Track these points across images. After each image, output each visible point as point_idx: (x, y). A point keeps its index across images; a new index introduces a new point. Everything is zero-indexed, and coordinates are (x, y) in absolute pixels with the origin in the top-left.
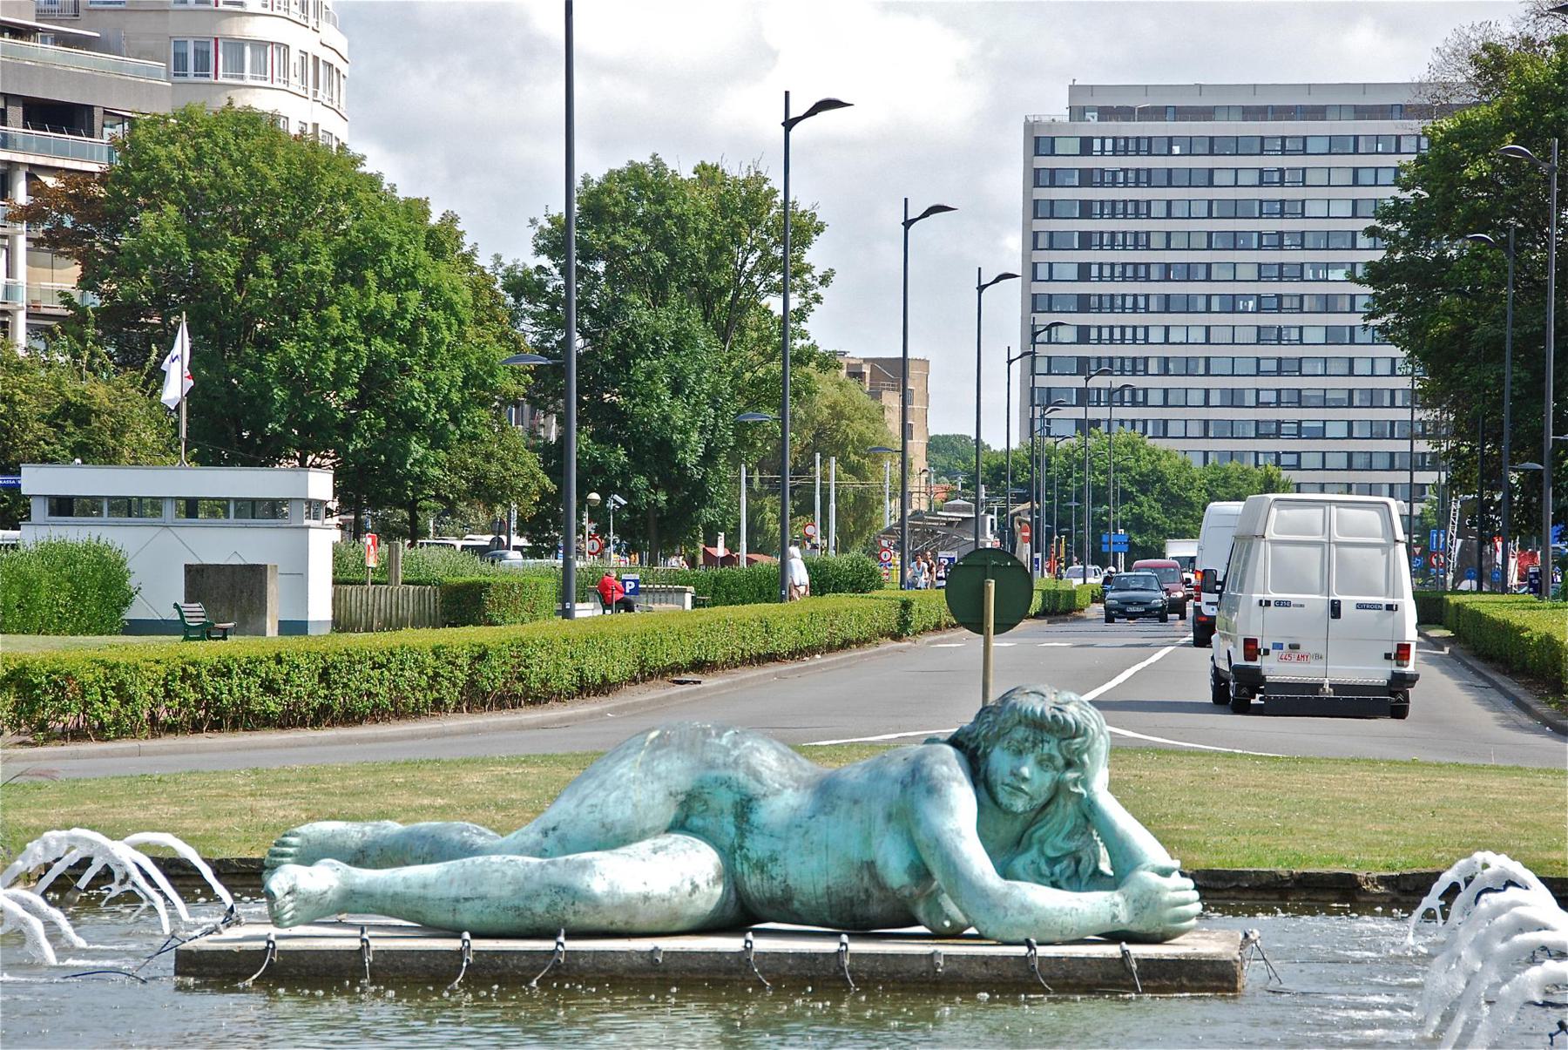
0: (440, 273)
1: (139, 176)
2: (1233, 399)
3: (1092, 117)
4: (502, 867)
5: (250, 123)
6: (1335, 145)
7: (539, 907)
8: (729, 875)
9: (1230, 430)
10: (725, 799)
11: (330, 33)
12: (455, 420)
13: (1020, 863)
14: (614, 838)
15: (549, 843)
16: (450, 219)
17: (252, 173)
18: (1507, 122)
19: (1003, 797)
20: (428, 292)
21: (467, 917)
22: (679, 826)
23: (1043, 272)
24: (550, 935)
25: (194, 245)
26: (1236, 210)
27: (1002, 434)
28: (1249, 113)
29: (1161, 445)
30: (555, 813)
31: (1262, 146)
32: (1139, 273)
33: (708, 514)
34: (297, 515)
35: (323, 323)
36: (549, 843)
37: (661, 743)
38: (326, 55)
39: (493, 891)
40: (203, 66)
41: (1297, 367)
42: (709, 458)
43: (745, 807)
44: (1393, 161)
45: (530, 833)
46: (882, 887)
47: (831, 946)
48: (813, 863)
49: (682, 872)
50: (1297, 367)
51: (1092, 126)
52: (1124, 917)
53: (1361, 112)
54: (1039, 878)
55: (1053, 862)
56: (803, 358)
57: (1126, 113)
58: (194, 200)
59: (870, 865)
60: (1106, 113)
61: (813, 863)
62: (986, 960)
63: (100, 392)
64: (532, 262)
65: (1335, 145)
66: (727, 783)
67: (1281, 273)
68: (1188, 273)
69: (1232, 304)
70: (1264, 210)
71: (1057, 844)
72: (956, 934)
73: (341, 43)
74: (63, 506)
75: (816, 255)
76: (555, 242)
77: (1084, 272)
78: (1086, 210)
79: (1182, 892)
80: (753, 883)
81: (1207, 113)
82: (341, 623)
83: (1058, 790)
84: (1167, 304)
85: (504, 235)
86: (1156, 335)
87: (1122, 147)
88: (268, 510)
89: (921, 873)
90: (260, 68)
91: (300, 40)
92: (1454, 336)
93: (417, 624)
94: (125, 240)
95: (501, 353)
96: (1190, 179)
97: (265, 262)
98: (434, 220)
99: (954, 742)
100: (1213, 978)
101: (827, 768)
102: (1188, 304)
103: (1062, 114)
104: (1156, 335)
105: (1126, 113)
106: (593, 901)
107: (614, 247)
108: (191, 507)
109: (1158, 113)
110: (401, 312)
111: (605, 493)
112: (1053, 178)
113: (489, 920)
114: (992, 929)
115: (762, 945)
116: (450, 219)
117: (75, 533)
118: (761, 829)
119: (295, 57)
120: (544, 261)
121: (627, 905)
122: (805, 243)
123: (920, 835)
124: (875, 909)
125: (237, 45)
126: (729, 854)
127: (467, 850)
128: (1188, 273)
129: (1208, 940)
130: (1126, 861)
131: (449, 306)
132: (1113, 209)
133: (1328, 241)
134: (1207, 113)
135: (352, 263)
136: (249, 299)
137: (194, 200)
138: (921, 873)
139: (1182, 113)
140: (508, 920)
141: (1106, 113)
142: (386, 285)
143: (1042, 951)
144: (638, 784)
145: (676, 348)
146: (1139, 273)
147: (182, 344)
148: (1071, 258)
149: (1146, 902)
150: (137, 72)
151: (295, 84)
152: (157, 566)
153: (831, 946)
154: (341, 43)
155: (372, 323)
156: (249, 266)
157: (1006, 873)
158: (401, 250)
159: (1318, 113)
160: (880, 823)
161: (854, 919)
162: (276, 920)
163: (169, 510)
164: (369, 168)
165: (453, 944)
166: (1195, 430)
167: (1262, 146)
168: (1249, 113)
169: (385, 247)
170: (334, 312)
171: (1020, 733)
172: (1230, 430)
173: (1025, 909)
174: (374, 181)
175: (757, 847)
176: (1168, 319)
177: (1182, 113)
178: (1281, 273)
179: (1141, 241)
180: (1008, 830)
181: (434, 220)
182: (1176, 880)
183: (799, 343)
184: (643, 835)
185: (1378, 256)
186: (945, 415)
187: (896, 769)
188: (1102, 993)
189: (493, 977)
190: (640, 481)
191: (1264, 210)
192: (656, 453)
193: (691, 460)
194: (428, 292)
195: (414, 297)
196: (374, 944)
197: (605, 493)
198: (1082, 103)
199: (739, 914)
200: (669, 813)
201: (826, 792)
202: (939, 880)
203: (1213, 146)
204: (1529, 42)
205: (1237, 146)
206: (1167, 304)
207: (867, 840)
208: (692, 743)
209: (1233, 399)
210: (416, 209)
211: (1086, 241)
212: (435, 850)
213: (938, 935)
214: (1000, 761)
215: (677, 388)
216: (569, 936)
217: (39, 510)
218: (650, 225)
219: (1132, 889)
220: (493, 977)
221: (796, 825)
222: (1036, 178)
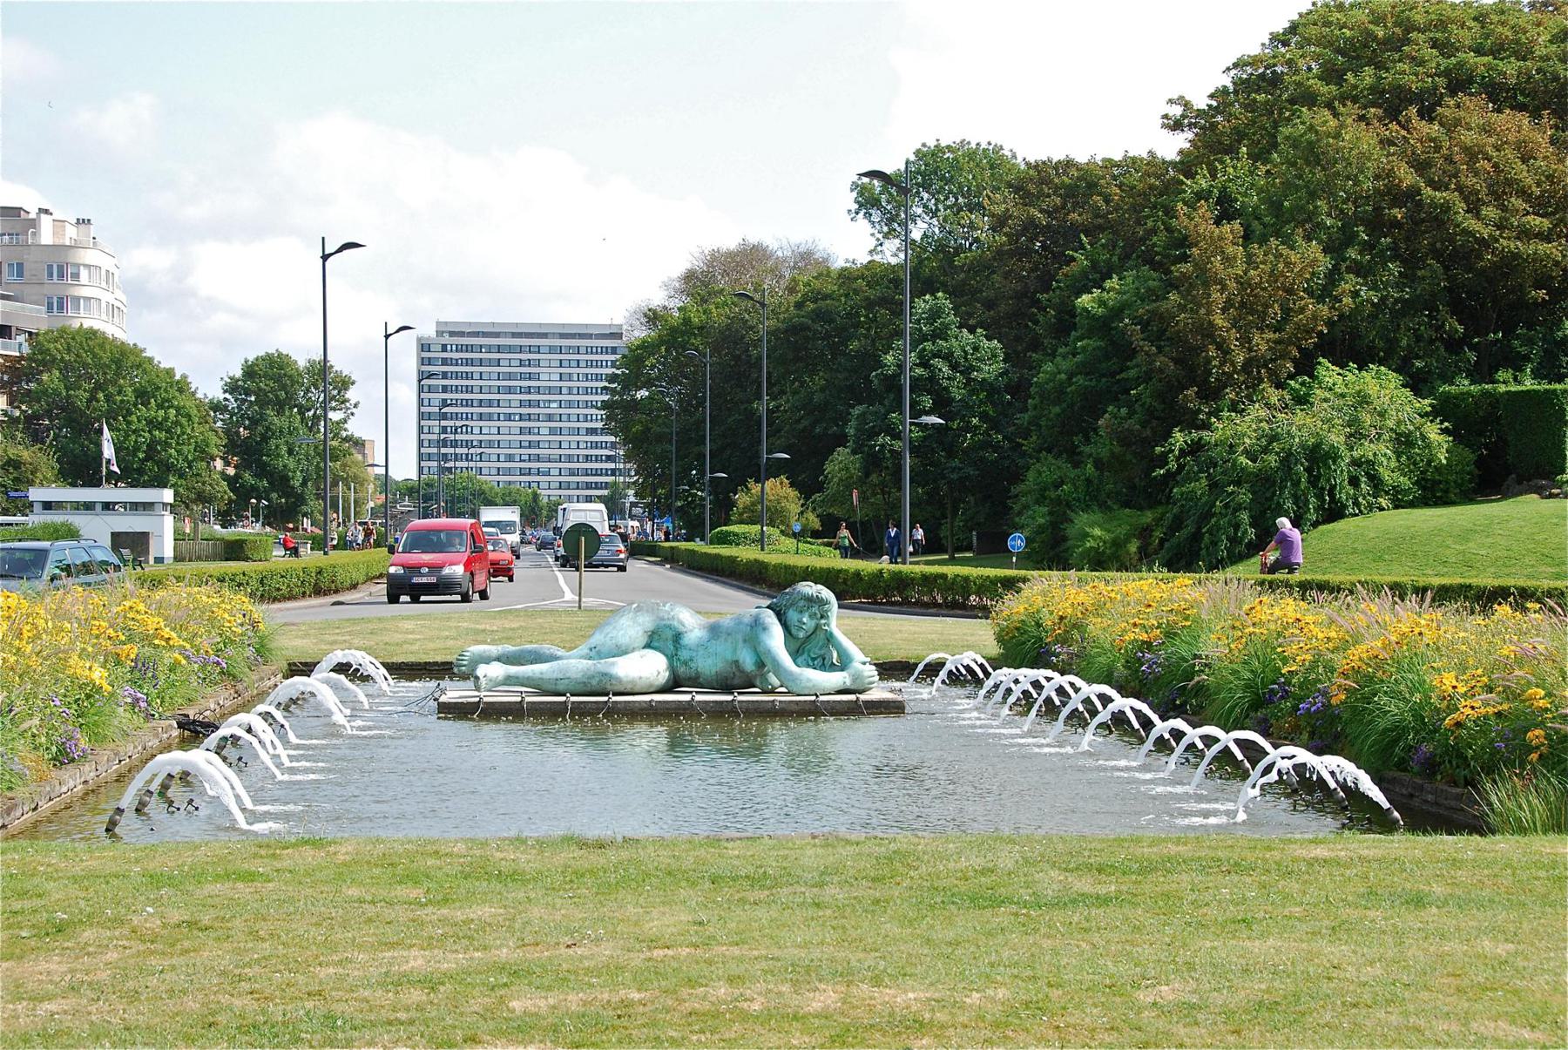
0: (180, 401)
2: (510, 458)
3: (446, 336)
4: (574, 665)
5: (92, 334)
6: (551, 350)
7: (594, 682)
8: (672, 668)
9: (509, 472)
10: (669, 634)
11: (119, 294)
12: (190, 467)
13: (799, 660)
14: (622, 651)
15: (593, 654)
16: (184, 377)
17: (95, 356)
18: (661, 341)
19: (794, 631)
20: (178, 409)
21: (561, 688)
22: (648, 646)
23: (426, 402)
24: (607, 694)
25: (67, 388)
26: (510, 376)
28: (514, 335)
29: (483, 478)
30: (597, 639)
31: (521, 349)
32: (470, 403)
33: (304, 508)
34: (158, 508)
35: (129, 423)
36: (593, 654)
37: (639, 609)
38: (117, 304)
39: (574, 676)
40: (61, 308)
41: (538, 445)
42: (304, 483)
43: (677, 637)
44: (613, 357)
45: (583, 649)
46: (742, 672)
47: (730, 698)
48: (710, 661)
49: (648, 667)
50: (538, 445)
51: (447, 339)
53: (563, 336)
55: (814, 659)
56: (347, 439)
57: (462, 334)
58: (66, 368)
59: (737, 662)
60: (452, 334)
61: (710, 661)
62: (797, 703)
63: (26, 455)
64: (222, 396)
65: (551, 350)
66: (669, 627)
67: (530, 404)
68: (490, 403)
69: (509, 417)
70: (522, 377)
71: (816, 652)
72: (772, 692)
73: (123, 298)
74: (48, 506)
75: (352, 394)
76: (232, 387)
78: (445, 375)
79: (871, 672)
80: (682, 670)
81: (497, 335)
82: (178, 558)
83: (817, 627)
84: (481, 417)
85: (210, 388)
86: (476, 431)
87: (460, 348)
88: (147, 506)
89: (761, 665)
90: (88, 309)
91: (106, 297)
92: (643, 432)
93: (208, 558)
94: (33, 386)
95: (212, 436)
96: (490, 363)
97: (101, 395)
98: (178, 377)
100: (892, 708)
101: (712, 620)
103: (433, 334)
104: (476, 431)
105: (462, 334)
106: (619, 680)
107: (260, 389)
108: (107, 506)
109: (476, 334)
110: (166, 419)
111: (259, 499)
112: (430, 362)
115: (699, 698)
116: (184, 377)
118: (685, 647)
119: (104, 305)
120: (228, 396)
121: (632, 682)
122: (346, 389)
123: (761, 649)
124: (736, 682)
125: (78, 298)
126: (670, 658)
127: (557, 658)
128: (490, 403)
129: (880, 692)
131: (189, 417)
132: (457, 376)
133: (550, 390)
134: (497, 335)
135: (143, 396)
136: (85, 411)
137: (66, 368)
138: (761, 665)
139: (485, 335)
140: (580, 688)
141: (452, 334)
142: (160, 406)
143: (822, 698)
144: (631, 628)
145: (290, 433)
146: (470, 403)
147: (106, 433)
149: (856, 677)
150: (31, 310)
151: (104, 317)
152: (97, 531)
153: (730, 698)
154: (123, 298)
155: (152, 424)
156: (93, 398)
158: (166, 391)
159: (545, 336)
160: (740, 644)
162: (478, 689)
163: (98, 507)
164: (148, 354)
165: (563, 699)
166: (494, 471)
167: (521, 349)
168: (514, 335)
169: (160, 389)
170: (134, 418)
171: (802, 603)
172: (509, 472)
173: (809, 680)
174: (150, 360)
175: (684, 654)
176: (482, 423)
177: (485, 335)
178: (530, 404)
179: (469, 389)
180: (794, 646)
181: (178, 377)
183: (344, 434)
184: (634, 650)
185: (606, 398)
187: (747, 620)
188: (498, 721)
189: (580, 712)
190: (274, 495)
191: (522, 377)
192: (280, 481)
193: (297, 484)
194: (178, 409)
195: (172, 412)
196: (528, 699)
197: (259, 499)
199: (672, 686)
200: (644, 640)
201: (714, 630)
202: (769, 666)
203: (499, 349)
204: (665, 308)
205: (510, 349)
206: (481, 417)
207: (735, 650)
208: (652, 610)
209: (510, 458)
210: (170, 372)
211: (445, 389)
212: (538, 658)
213: (764, 692)
214: (792, 615)
215: (290, 452)
216: (615, 694)
217: (37, 508)
218: (278, 379)
219: (851, 671)
220: (580, 712)
221: (701, 645)
222: (422, 361)
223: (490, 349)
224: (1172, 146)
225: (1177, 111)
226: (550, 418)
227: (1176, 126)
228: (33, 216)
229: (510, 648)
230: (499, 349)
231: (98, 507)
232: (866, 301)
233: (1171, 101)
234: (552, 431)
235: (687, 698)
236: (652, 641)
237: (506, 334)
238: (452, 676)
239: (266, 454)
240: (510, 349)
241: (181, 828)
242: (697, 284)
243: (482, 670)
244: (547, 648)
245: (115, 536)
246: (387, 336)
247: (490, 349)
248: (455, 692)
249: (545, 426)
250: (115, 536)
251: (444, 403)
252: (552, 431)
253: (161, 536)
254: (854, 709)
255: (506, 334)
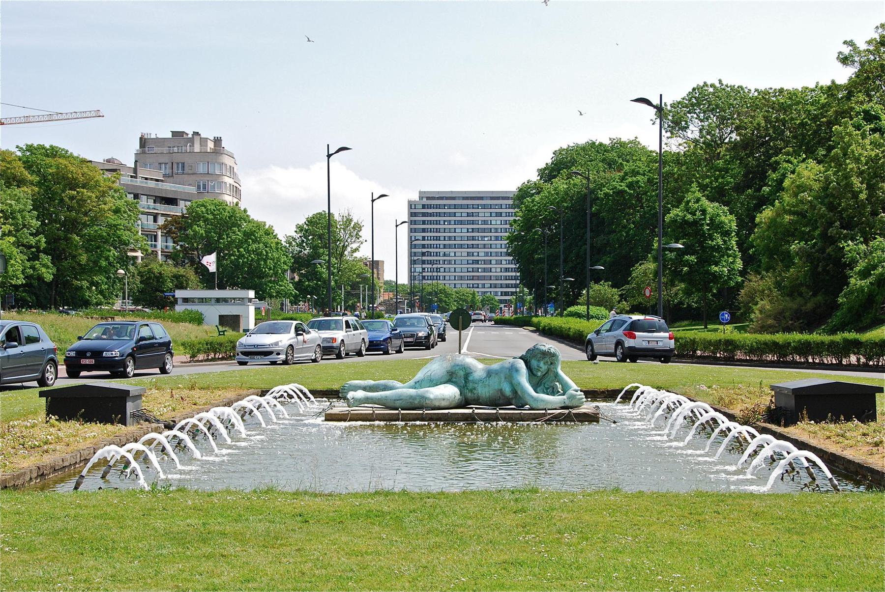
1: (193, 217)
3: (425, 199)
6: (484, 207)
10: (462, 373)
21: (398, 404)
27: (404, 279)
28: (464, 198)
31: (467, 207)
47: (495, 411)
48: (487, 390)
51: (425, 201)
52: (568, 403)
53: (492, 198)
54: (544, 393)
55: (547, 389)
60: (428, 198)
61: (487, 390)
74: (186, 300)
77: (424, 238)
78: (424, 222)
80: (469, 395)
81: (454, 198)
83: (548, 370)
96: (450, 215)
98: (267, 227)
99: (520, 358)
100: (592, 418)
102: (450, 246)
108: (218, 300)
113: (404, 404)
114: (534, 406)
115: (500, 411)
117: (189, 307)
124: (501, 402)
129: (588, 407)
130: (565, 388)
132: (430, 222)
134: (454, 198)
139: (447, 198)
140: (408, 405)
141: (428, 198)
148: (420, 235)
149: (572, 397)
153: (495, 411)
157: (537, 392)
161: (493, 403)
167: (467, 207)
169: (258, 234)
175: (470, 385)
177: (447, 198)
180: (535, 380)
181: (267, 227)
182: (579, 393)
186: (388, 275)
198: (422, 195)
203: (455, 206)
205: (461, 207)
212: (386, 388)
217: (180, 301)
223: (450, 207)
224: (844, 75)
225: (846, 50)
226: (484, 246)
227: (845, 60)
228: (190, 136)
229: (371, 382)
230: (455, 206)
231: (213, 301)
232: (671, 176)
233: (845, 42)
234: (486, 254)
235: (470, 411)
236: (450, 378)
237: (487, 198)
238: (339, 398)
239: (316, 272)
240: (461, 207)
241: (125, 485)
242: (561, 165)
243: (351, 395)
244: (391, 383)
245: (221, 317)
246: (373, 201)
247: (450, 207)
248: (339, 407)
249: (482, 251)
250: (221, 317)
251: (424, 238)
252: (486, 254)
253: (248, 317)
254: (570, 417)
255: (487, 198)
